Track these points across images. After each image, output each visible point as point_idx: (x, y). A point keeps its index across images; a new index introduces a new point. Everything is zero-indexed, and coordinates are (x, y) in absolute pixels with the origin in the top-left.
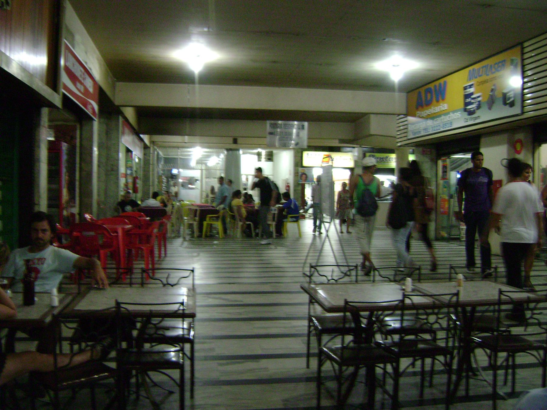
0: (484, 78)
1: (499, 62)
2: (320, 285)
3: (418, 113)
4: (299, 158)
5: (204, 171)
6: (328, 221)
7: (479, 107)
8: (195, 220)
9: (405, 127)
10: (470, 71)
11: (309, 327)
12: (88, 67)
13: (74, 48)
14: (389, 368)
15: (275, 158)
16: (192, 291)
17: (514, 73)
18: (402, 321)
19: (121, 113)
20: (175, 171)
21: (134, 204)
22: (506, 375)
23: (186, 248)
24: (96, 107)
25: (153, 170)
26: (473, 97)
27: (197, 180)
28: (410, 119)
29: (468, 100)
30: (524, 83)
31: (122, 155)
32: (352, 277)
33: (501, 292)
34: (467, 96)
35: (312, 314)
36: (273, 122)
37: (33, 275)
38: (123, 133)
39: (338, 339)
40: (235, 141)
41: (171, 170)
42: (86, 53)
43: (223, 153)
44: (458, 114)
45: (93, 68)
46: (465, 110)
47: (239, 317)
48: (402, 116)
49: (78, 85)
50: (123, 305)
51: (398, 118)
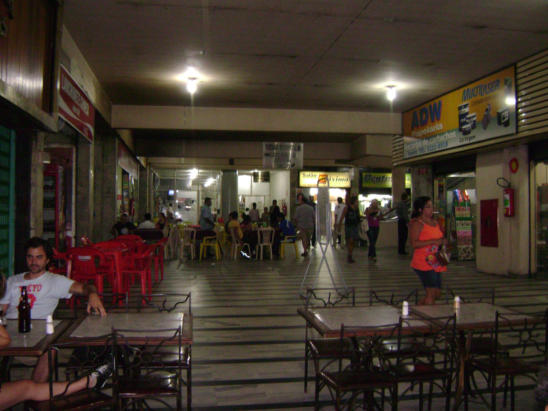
0: (479, 97)
1: (493, 82)
2: (317, 310)
3: (414, 133)
4: (296, 179)
5: (200, 192)
6: (325, 242)
7: (474, 127)
8: (192, 242)
9: (401, 147)
10: (464, 91)
11: (307, 351)
12: (84, 91)
13: (70, 72)
14: (387, 393)
15: (271, 179)
16: (189, 316)
17: (508, 92)
18: (399, 344)
19: (118, 136)
20: (171, 192)
21: (130, 226)
22: (505, 397)
23: (183, 270)
24: (92, 130)
25: (150, 191)
26: (468, 116)
27: (193, 202)
28: (406, 139)
29: (463, 120)
30: (517, 103)
31: (118, 177)
32: (349, 299)
33: (498, 315)
34: (462, 116)
35: (309, 337)
36: (269, 143)
37: (29, 301)
38: (119, 155)
39: (336, 365)
40: (231, 162)
41: (168, 192)
42: (82, 76)
43: (220, 174)
44: (454, 134)
45: (89, 92)
46: (460, 130)
47: (237, 341)
48: (398, 136)
49: (74, 108)
50: (118, 333)
51: (394, 138)
